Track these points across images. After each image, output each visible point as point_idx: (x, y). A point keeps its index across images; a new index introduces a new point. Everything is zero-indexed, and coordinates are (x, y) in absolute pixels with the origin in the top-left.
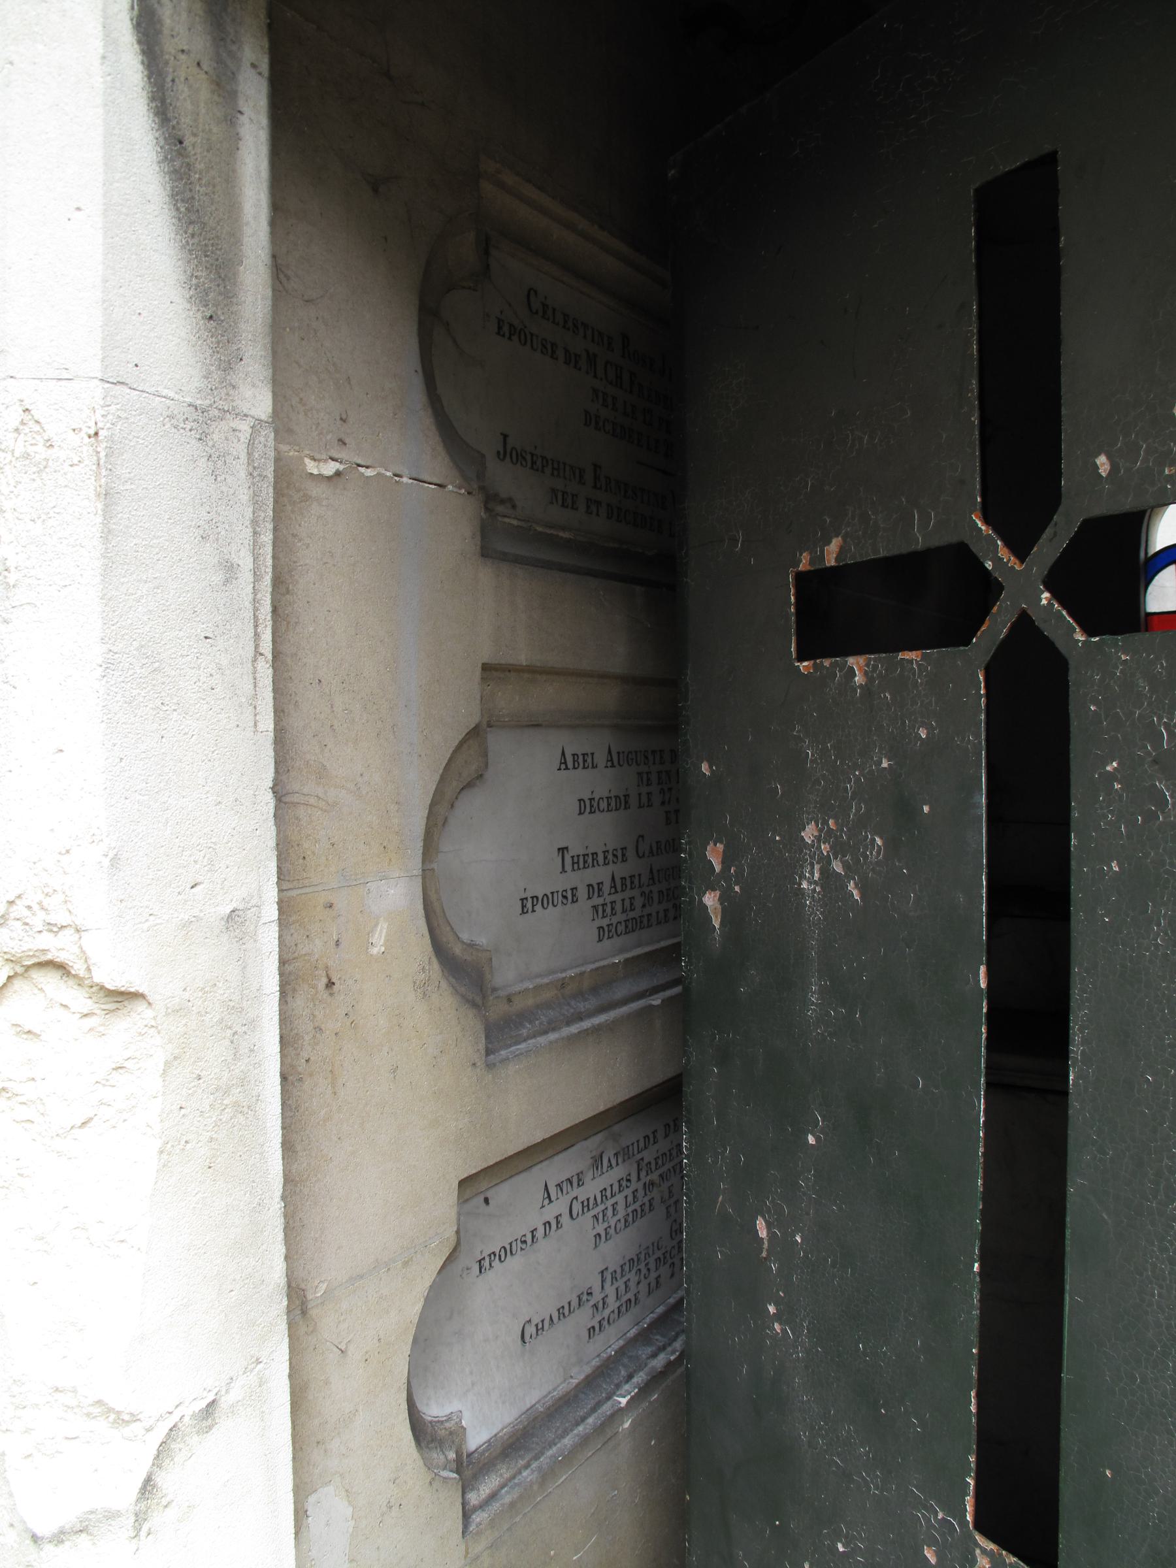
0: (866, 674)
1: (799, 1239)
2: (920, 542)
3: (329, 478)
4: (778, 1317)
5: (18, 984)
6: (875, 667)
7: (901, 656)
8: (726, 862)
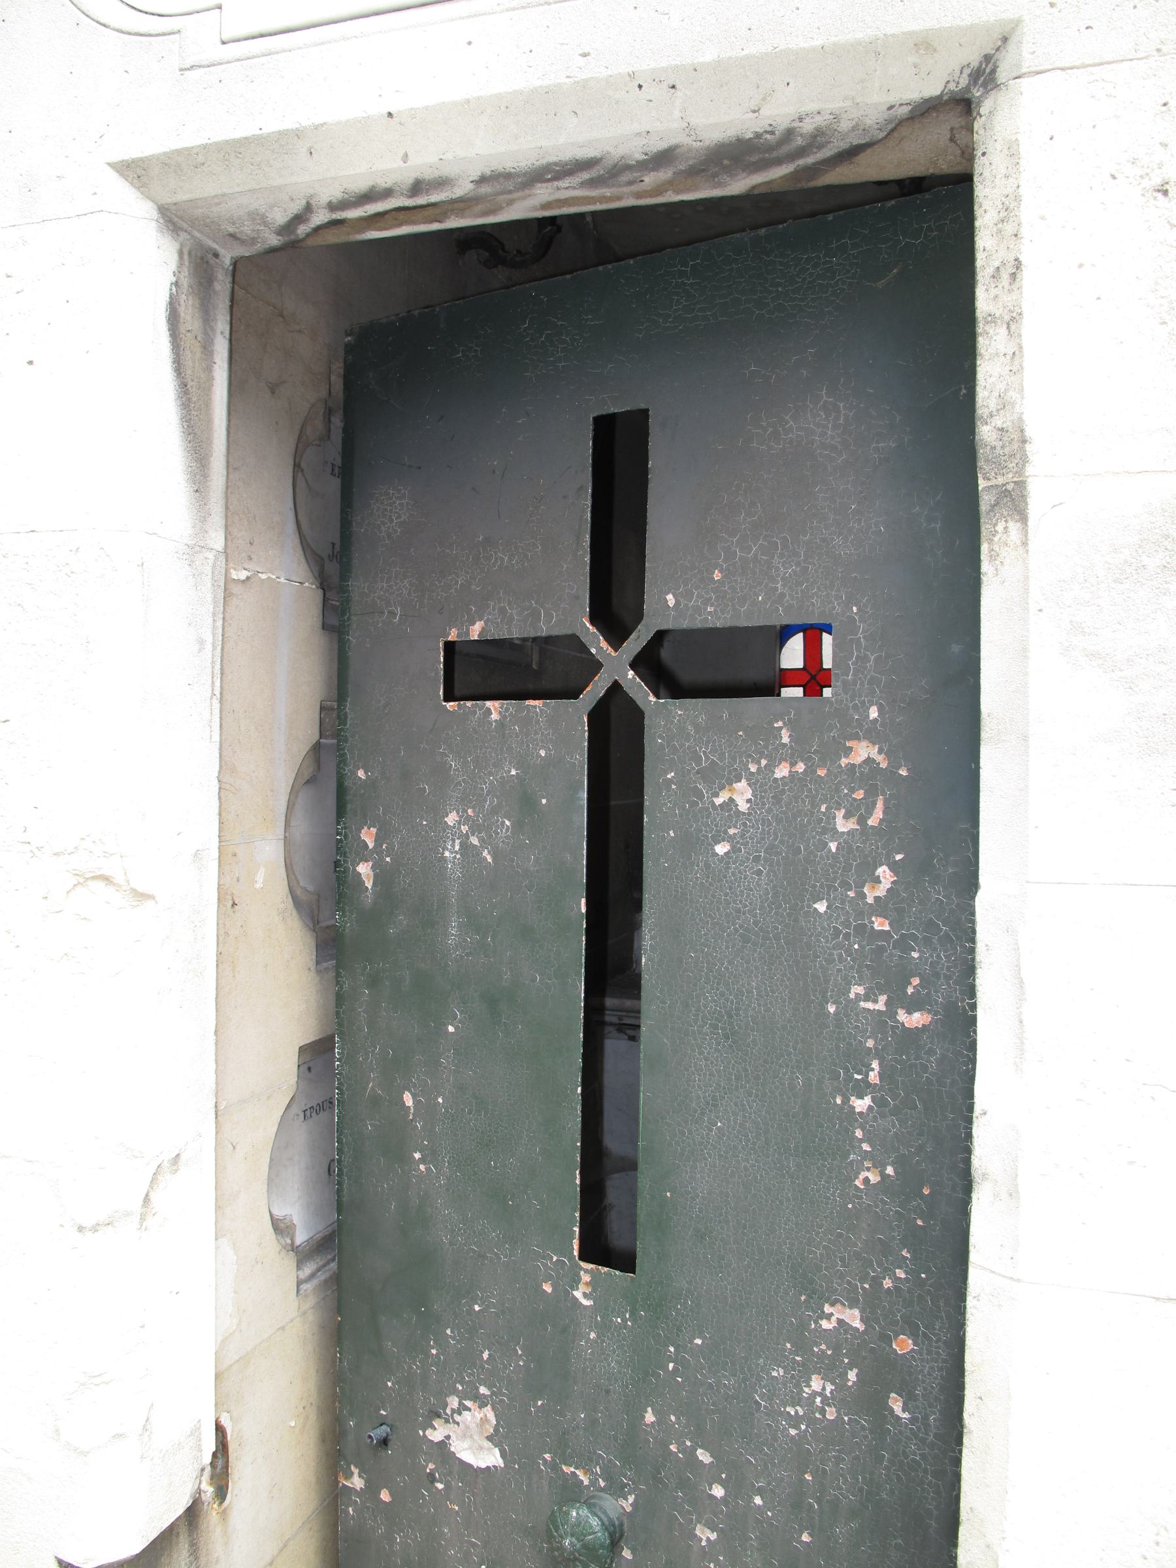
1: (440, 1100)
3: (243, 581)
5: (79, 889)
6: (507, 710)
7: (527, 702)
8: (378, 840)
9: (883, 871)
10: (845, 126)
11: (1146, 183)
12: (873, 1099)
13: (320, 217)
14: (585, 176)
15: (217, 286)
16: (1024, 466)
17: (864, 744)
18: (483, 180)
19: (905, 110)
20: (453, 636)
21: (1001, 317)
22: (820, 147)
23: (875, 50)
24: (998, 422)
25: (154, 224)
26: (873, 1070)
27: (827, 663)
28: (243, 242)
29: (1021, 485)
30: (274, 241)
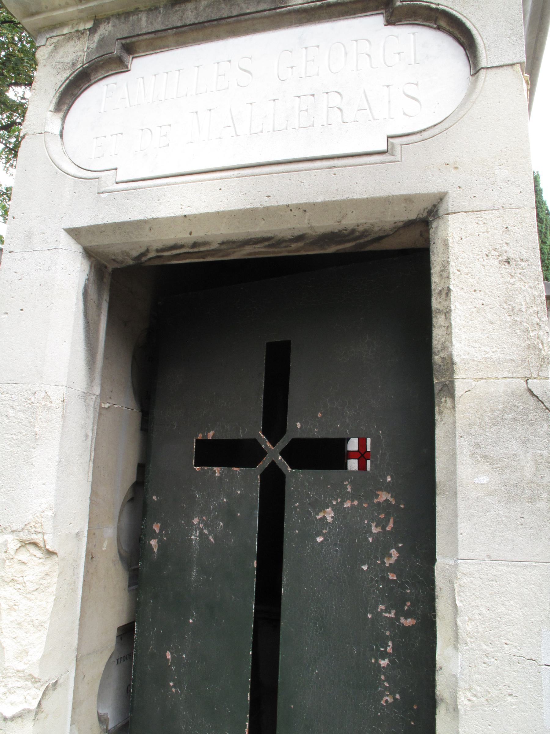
0: (220, 473)
1: (184, 656)
2: (241, 436)
3: (107, 408)
4: (174, 686)
5: (21, 549)
6: (223, 471)
7: (233, 469)
8: (161, 530)
9: (393, 551)
10: (376, 229)
11: (500, 258)
12: (389, 661)
13: (152, 255)
14: (267, 243)
15: (105, 280)
16: (453, 374)
17: (385, 493)
18: (223, 243)
19: (401, 224)
20: (200, 437)
21: (442, 311)
22: (366, 236)
23: (388, 201)
24: (442, 355)
25: (81, 254)
26: (389, 646)
27: (369, 449)
28: (118, 262)
29: (452, 382)
30: (131, 262)
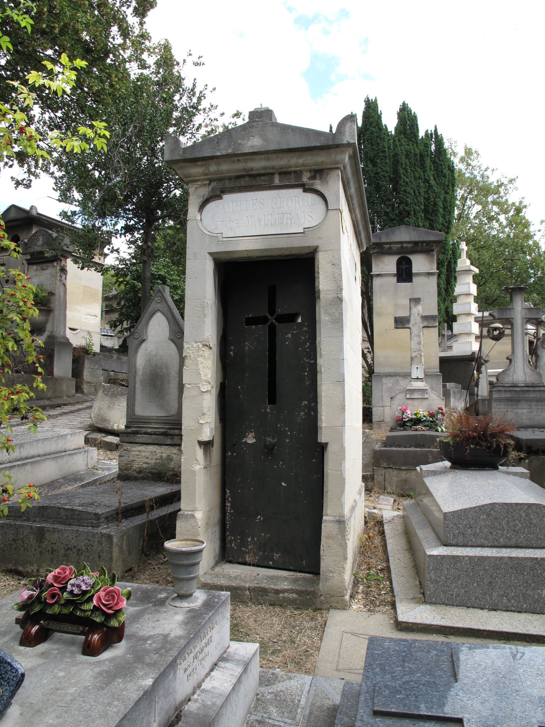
20: (247, 316)
23: (304, 247)
